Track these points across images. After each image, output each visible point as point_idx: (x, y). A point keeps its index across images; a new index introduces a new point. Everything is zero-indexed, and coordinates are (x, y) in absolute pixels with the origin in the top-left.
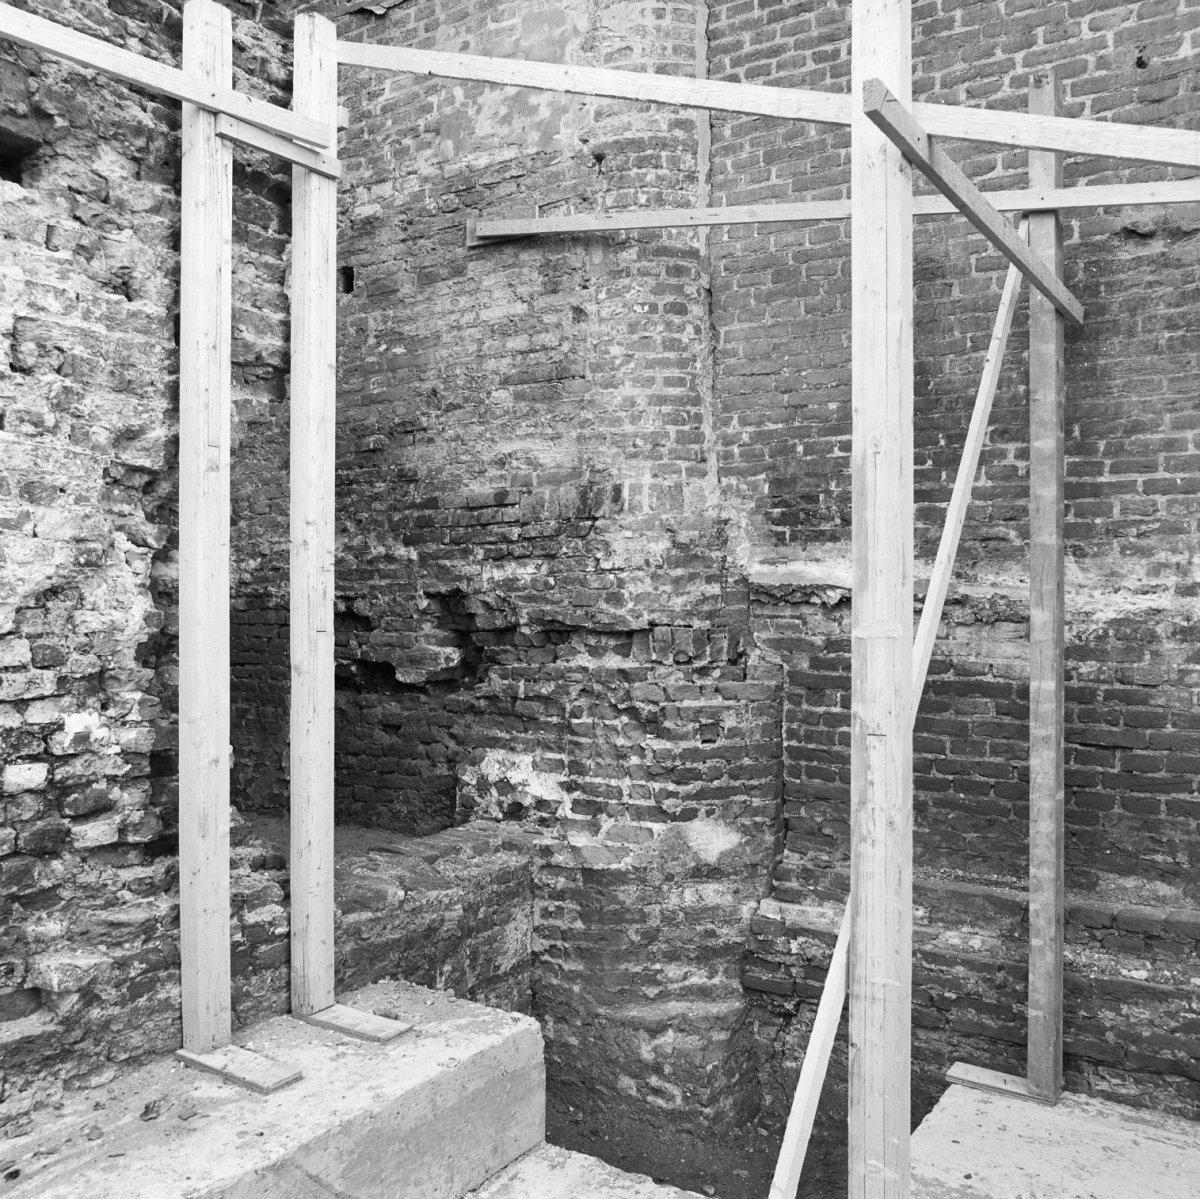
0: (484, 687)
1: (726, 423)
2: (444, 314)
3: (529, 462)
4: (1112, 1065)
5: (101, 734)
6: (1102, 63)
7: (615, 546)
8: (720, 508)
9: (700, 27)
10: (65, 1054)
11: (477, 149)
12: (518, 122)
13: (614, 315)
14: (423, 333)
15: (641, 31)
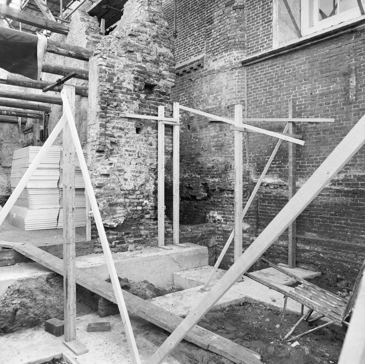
0: (210, 200)
1: (250, 154)
2: (204, 134)
3: (217, 161)
4: (303, 263)
5: (148, 203)
6: (306, 94)
7: (230, 176)
8: (249, 169)
9: (246, 83)
10: (144, 243)
11: (209, 105)
12: (216, 101)
13: (231, 135)
14: (201, 137)
15: (235, 85)
